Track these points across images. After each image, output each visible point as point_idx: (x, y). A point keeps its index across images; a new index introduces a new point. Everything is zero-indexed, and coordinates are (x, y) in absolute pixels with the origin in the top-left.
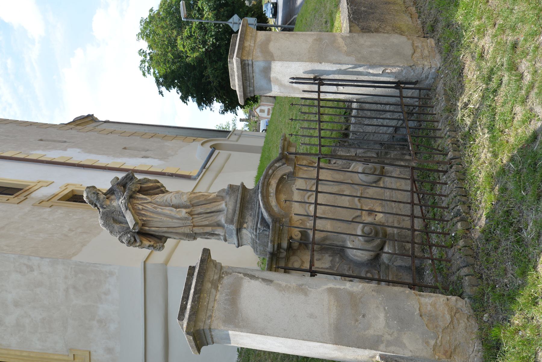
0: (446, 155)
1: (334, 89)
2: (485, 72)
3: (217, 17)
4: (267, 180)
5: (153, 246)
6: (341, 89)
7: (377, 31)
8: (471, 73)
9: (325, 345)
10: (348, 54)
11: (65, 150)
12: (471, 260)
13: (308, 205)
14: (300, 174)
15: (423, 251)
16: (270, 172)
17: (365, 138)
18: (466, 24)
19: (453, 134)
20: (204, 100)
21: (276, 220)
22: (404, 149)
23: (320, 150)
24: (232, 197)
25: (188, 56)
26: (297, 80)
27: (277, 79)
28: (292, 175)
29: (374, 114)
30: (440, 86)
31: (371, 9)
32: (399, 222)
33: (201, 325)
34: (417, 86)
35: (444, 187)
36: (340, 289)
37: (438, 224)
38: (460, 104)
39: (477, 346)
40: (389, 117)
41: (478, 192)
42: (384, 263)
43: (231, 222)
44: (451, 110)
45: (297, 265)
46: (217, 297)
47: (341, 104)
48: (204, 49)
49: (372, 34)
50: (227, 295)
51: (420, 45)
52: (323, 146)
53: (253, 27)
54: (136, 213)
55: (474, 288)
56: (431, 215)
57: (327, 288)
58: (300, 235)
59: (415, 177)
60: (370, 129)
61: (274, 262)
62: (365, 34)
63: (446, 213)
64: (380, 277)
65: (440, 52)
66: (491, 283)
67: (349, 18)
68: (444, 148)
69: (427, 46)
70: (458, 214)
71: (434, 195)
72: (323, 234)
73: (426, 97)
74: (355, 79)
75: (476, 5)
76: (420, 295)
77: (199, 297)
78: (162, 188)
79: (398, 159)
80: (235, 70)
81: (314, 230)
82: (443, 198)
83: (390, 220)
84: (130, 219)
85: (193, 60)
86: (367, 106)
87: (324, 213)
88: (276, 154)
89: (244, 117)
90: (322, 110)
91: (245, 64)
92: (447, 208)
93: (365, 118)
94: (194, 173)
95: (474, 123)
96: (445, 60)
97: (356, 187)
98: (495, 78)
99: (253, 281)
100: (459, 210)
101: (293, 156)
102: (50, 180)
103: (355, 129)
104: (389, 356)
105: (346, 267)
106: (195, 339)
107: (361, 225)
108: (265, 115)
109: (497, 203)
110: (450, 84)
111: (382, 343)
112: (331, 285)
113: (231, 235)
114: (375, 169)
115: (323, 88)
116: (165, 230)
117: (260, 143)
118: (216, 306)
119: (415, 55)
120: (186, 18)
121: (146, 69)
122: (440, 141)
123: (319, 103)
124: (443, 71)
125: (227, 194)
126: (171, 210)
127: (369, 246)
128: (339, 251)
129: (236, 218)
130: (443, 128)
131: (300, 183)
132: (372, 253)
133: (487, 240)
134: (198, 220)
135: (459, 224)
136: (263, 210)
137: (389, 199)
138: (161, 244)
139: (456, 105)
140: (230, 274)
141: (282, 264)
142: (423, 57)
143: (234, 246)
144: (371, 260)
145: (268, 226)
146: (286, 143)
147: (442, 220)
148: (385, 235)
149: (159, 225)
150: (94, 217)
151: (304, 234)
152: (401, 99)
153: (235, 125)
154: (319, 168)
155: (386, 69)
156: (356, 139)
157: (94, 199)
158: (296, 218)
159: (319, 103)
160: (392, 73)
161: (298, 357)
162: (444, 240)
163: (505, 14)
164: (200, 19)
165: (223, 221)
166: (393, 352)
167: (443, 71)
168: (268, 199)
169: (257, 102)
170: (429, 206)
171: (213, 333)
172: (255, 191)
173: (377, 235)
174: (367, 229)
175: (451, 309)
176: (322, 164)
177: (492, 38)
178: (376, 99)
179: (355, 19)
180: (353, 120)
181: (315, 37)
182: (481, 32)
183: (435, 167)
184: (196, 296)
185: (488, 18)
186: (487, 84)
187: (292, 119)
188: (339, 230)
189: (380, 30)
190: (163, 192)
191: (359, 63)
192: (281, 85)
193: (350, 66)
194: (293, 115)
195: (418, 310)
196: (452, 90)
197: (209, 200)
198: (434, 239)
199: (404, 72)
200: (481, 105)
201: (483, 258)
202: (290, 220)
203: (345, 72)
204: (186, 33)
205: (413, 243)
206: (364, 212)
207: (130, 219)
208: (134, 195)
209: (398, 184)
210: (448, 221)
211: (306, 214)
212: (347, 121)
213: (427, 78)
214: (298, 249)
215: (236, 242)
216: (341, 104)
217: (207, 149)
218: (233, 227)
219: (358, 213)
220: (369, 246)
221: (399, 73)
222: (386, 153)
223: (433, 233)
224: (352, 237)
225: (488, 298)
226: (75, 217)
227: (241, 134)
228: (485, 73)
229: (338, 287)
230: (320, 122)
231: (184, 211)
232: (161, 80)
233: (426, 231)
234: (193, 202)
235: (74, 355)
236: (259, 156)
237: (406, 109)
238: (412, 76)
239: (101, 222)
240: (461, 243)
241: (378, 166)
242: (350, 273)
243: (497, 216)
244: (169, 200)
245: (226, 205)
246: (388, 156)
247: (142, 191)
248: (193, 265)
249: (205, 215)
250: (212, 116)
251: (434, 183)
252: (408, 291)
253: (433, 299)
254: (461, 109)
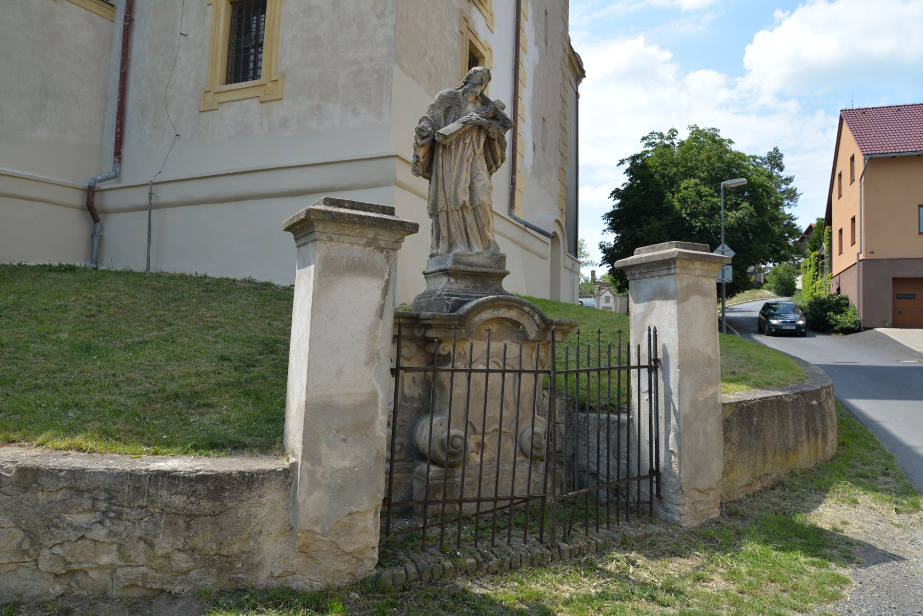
0: (564, 541)
1: (645, 387)
2: (679, 585)
3: (730, 230)
4: (515, 304)
5: (418, 161)
6: (645, 397)
7: (727, 440)
8: (675, 567)
9: (304, 391)
10: (693, 403)
11: (536, 43)
12: (426, 576)
13: (485, 362)
14: (526, 350)
15: (435, 516)
16: (527, 309)
17: (580, 434)
18: (741, 556)
19: (593, 549)
20: (616, 220)
21: (463, 320)
22: (569, 486)
23: (560, 373)
24: (489, 261)
25: (674, 195)
26: (653, 336)
27: (652, 310)
28: (523, 337)
29: (613, 443)
30: (657, 529)
31: (756, 431)
32: (470, 484)
33: (319, 228)
34: (655, 498)
35: (521, 540)
37: (471, 534)
38: (633, 555)
39: (318, 585)
40: (611, 463)
41: (516, 584)
42: (415, 467)
43: (456, 262)
44: (625, 545)
45: (405, 351)
46: (356, 247)
47: (624, 399)
48: (684, 215)
49: (722, 433)
50: (360, 259)
51: (711, 498)
52: (566, 377)
53: (720, 277)
54: (460, 136)
55: (390, 582)
56: (482, 524)
58: (444, 353)
59: (531, 503)
60: (593, 439)
61: (406, 321)
62: (721, 424)
63: (485, 544)
64: (397, 461)
65: (702, 526)
66: (399, 602)
67: (741, 402)
68: (573, 537)
69: (710, 508)
70: (486, 559)
71: (509, 527)
72: (447, 384)
73: (641, 512)
74: (660, 415)
75: (767, 567)
76: (376, 512)
77: (354, 223)
78: (494, 168)
79: (554, 477)
80: (661, 252)
81: (453, 371)
82: (506, 539)
83: (472, 472)
84: (452, 128)
85: (669, 201)
86: (624, 434)
87: (476, 384)
88: (550, 316)
89: (598, 276)
90: (614, 373)
91: (670, 264)
92: (493, 545)
93: (608, 432)
94: (517, 213)
95: (609, 574)
96: (692, 532)
97: (514, 425)
98: (670, 597)
99: (380, 292)
100: (491, 560)
101: (549, 338)
102: (496, 29)
103: (591, 420)
104: (296, 474)
105: (406, 417)
106: (301, 222)
107: (463, 434)
108: (603, 304)
109: (503, 607)
110: (660, 541)
111: (313, 465)
112: (381, 395)
113: (439, 263)
114: (539, 449)
115: (644, 372)
116: (440, 175)
117: (565, 298)
118: (345, 246)
119: (697, 493)
120: (725, 188)
121: (652, 141)
122: (582, 532)
123: (624, 368)
124: (677, 531)
125: (493, 254)
126: (466, 181)
127: (436, 446)
128: (427, 407)
129: (462, 267)
130: (600, 535)
131: (513, 349)
132: (427, 450)
133: (454, 596)
134: (456, 217)
135: (472, 561)
136: (475, 302)
137: (500, 466)
138: (421, 172)
139: (632, 550)
140: (388, 262)
141: (405, 332)
142: (694, 504)
143: (424, 268)
144: (418, 449)
145: (454, 309)
146: (567, 327)
147: (477, 538)
148: (453, 466)
149: (446, 167)
150: (450, 84)
151: (447, 358)
152: (635, 479)
153: (586, 264)
154: (536, 373)
155: (675, 455)
156: (579, 422)
157: (475, 80)
158: (467, 346)
159: (624, 368)
160: (671, 463)
161: (287, 361)
162: (451, 542)
163: (756, 604)
164: (725, 208)
165: (457, 250)
166: (301, 479)
167: (677, 531)
168: (490, 307)
169: (619, 292)
170: (494, 521)
171: (310, 245)
172: (500, 291)
173: (451, 456)
174: (459, 442)
175: (361, 552)
176: (541, 375)
177: (724, 591)
178: (634, 445)
179: (741, 410)
180: (604, 416)
181: (713, 357)
182: (732, 576)
183: (546, 528)
184: (356, 219)
185: (751, 583)
186: (662, 588)
187: (599, 332)
188: (454, 405)
189: (728, 445)
190: (489, 169)
191: (681, 418)
192: (645, 316)
193: (677, 407)
194: (606, 337)
195: (358, 509)
196: (652, 544)
197: (483, 230)
198: (451, 530)
199: (674, 480)
200: (634, 582)
201: (431, 591)
202: (464, 340)
203: (668, 401)
204: (704, 189)
205: (444, 502)
206: (481, 437)
207: (452, 128)
208: (483, 132)
209: (521, 481)
210: (476, 546)
211: (473, 359)
212: (602, 409)
213: (667, 510)
214: (427, 353)
215: (429, 270)
216: (624, 399)
217: (551, 228)
218: (449, 264)
219: (479, 429)
220: (436, 446)
221: (671, 474)
222: (561, 463)
223: (459, 528)
224: (447, 422)
225: (379, 598)
226: (449, 63)
227: (575, 272)
228: (677, 585)
229: (380, 405)
230: (599, 370)
231: (467, 198)
232: (639, 161)
233: (461, 519)
234: (479, 208)
236: (548, 298)
237: (623, 485)
238: (669, 490)
239: (444, 91)
240: (448, 564)
241: (544, 453)
242: (399, 423)
243: (486, 607)
244: (479, 177)
245: (478, 253)
246: (558, 466)
247: (489, 141)
248: (396, 211)
249: (462, 227)
250: (595, 234)
251: (525, 527)
252: (381, 496)
253: (372, 529)
254: (627, 557)
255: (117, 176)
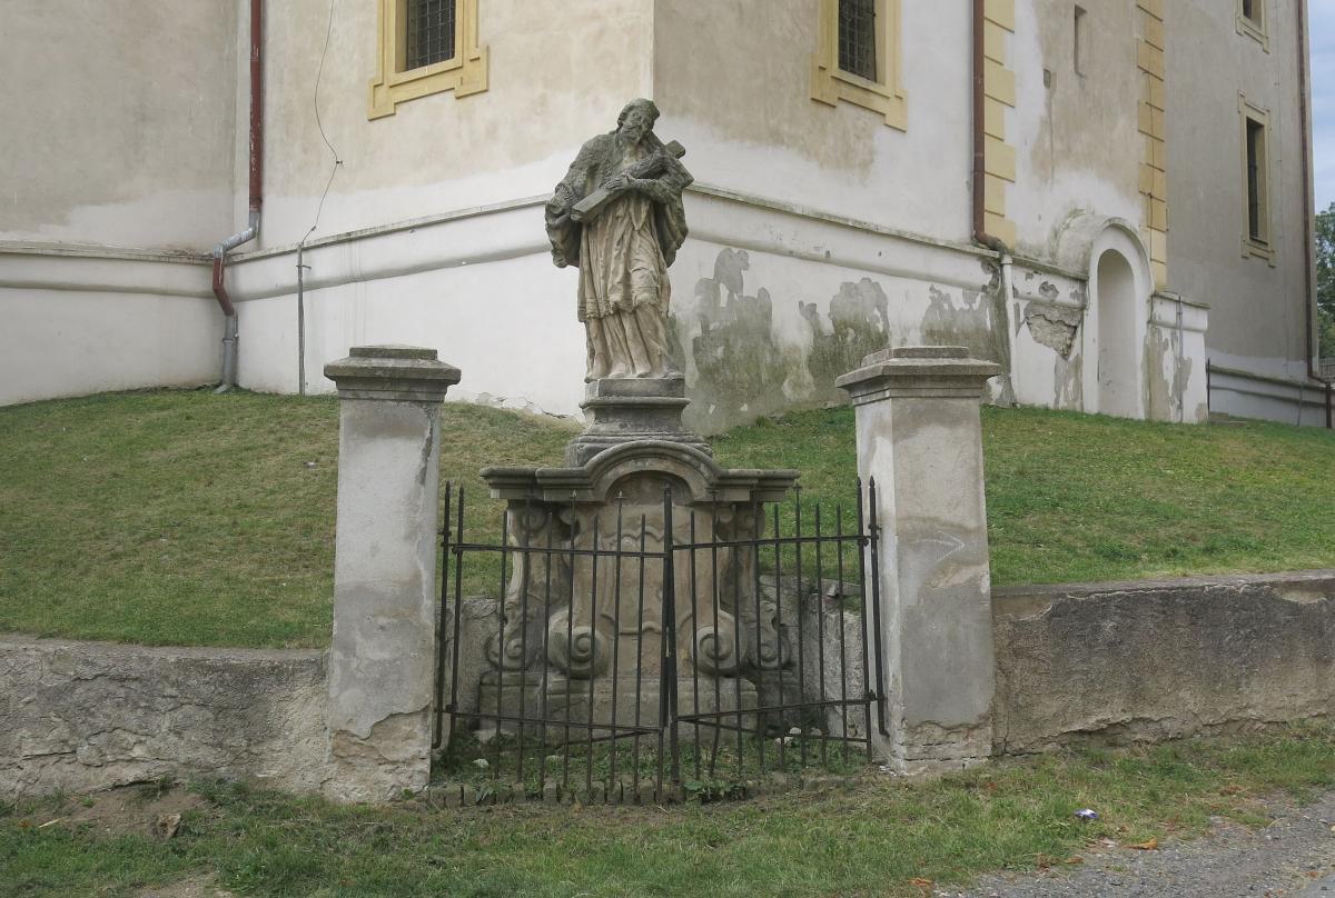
23: (680, 547)
36: (421, 590)
57: (419, 571)
99: (420, 453)
111: (345, 655)
129: (613, 399)
154: (714, 546)
229: (425, 586)
235: (479, 58)
255: (256, 234)
